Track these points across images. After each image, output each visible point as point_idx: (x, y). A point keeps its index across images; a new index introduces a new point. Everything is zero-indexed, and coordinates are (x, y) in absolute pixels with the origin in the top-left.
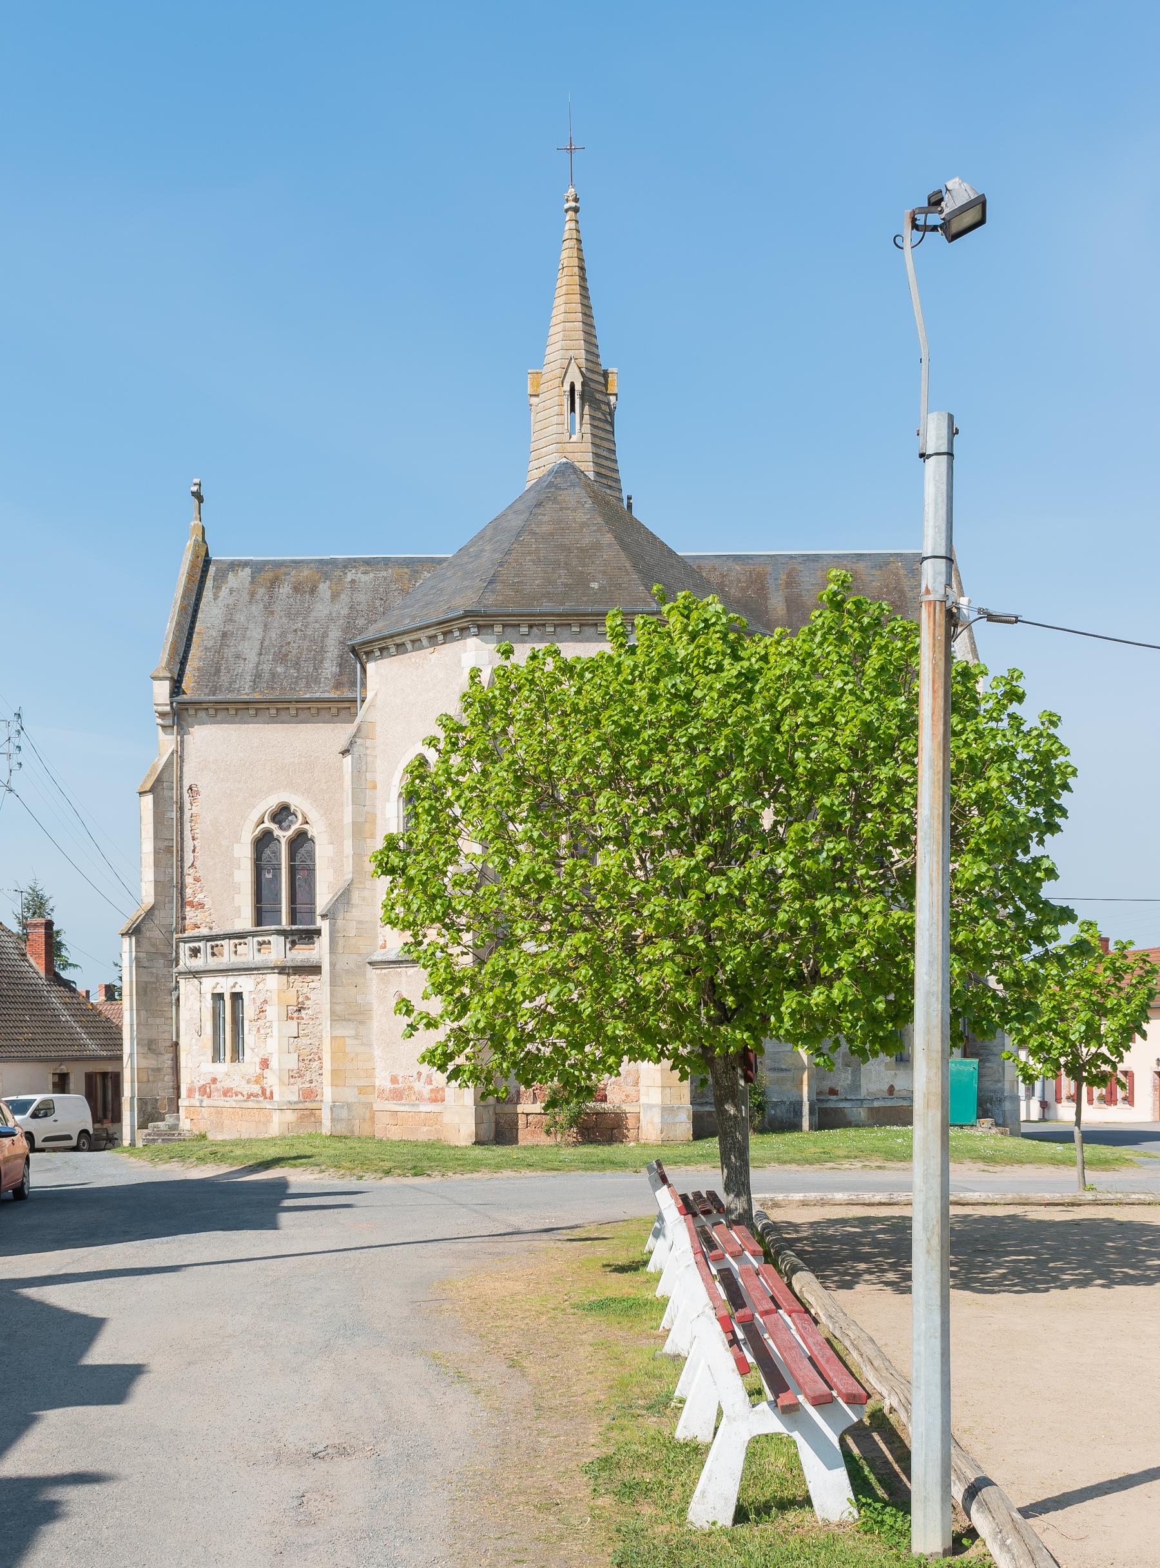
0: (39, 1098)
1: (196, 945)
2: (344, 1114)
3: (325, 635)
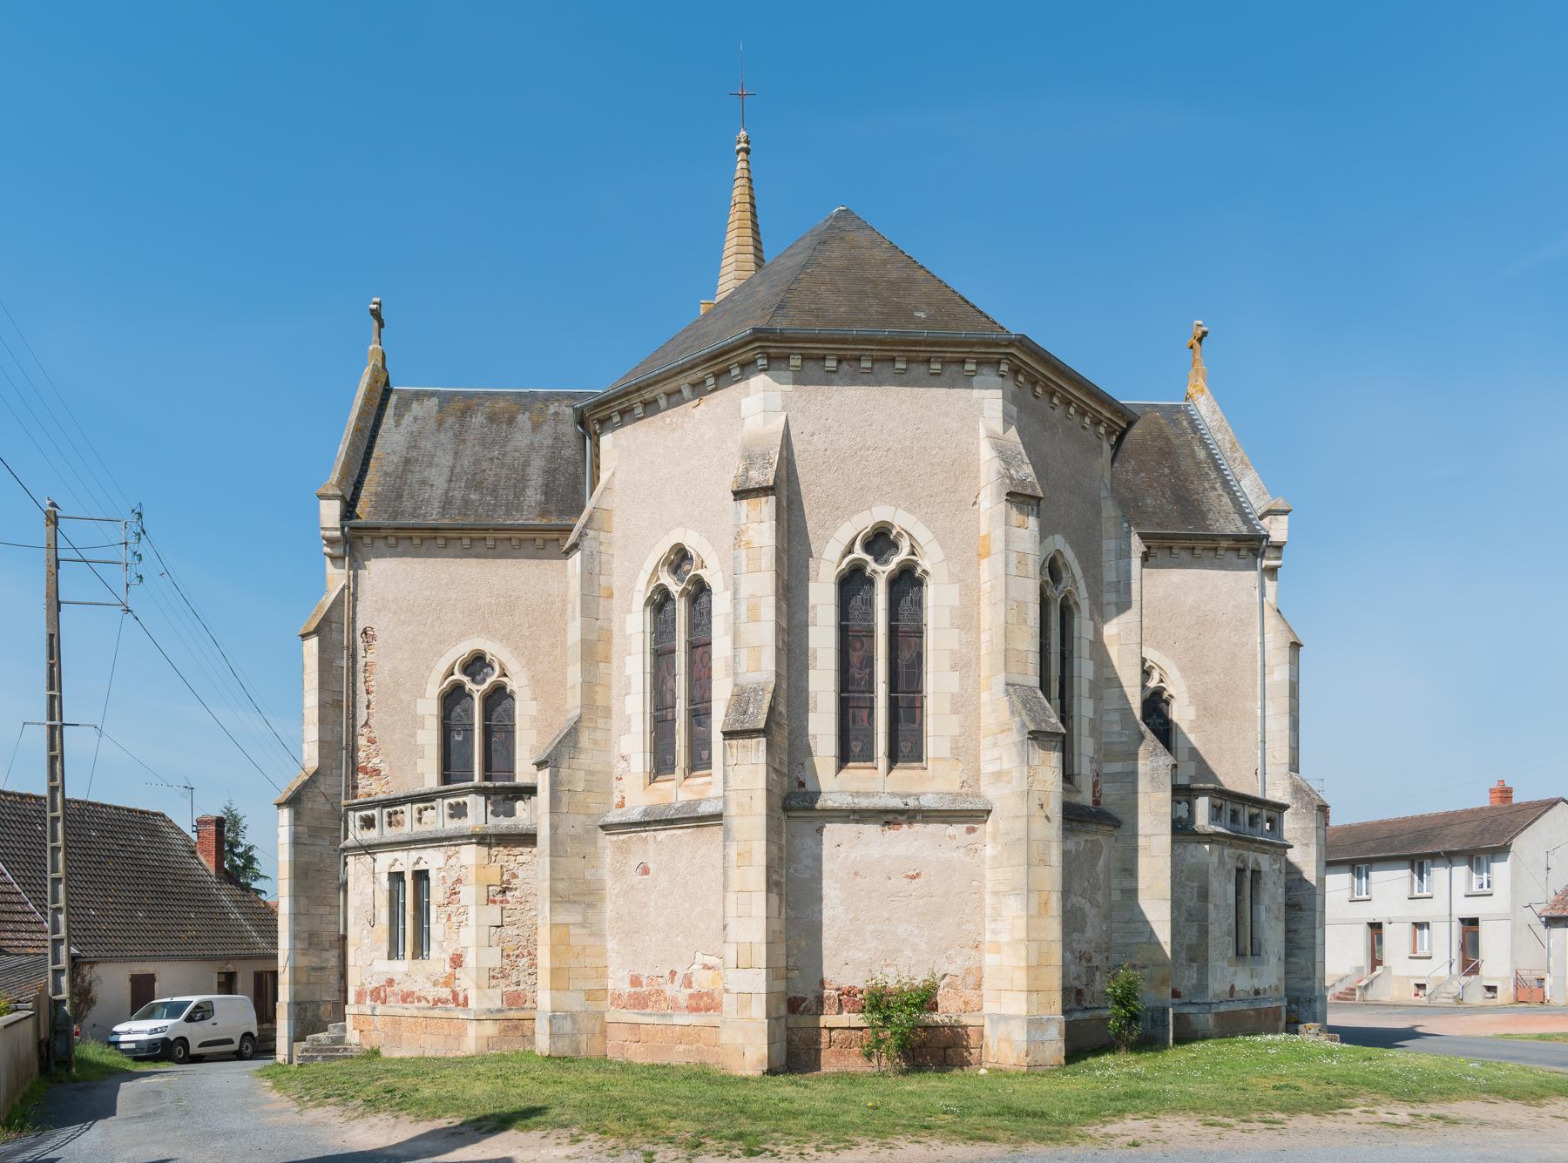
0: (195, 999)
1: (369, 812)
2: (567, 1026)
3: (526, 464)
